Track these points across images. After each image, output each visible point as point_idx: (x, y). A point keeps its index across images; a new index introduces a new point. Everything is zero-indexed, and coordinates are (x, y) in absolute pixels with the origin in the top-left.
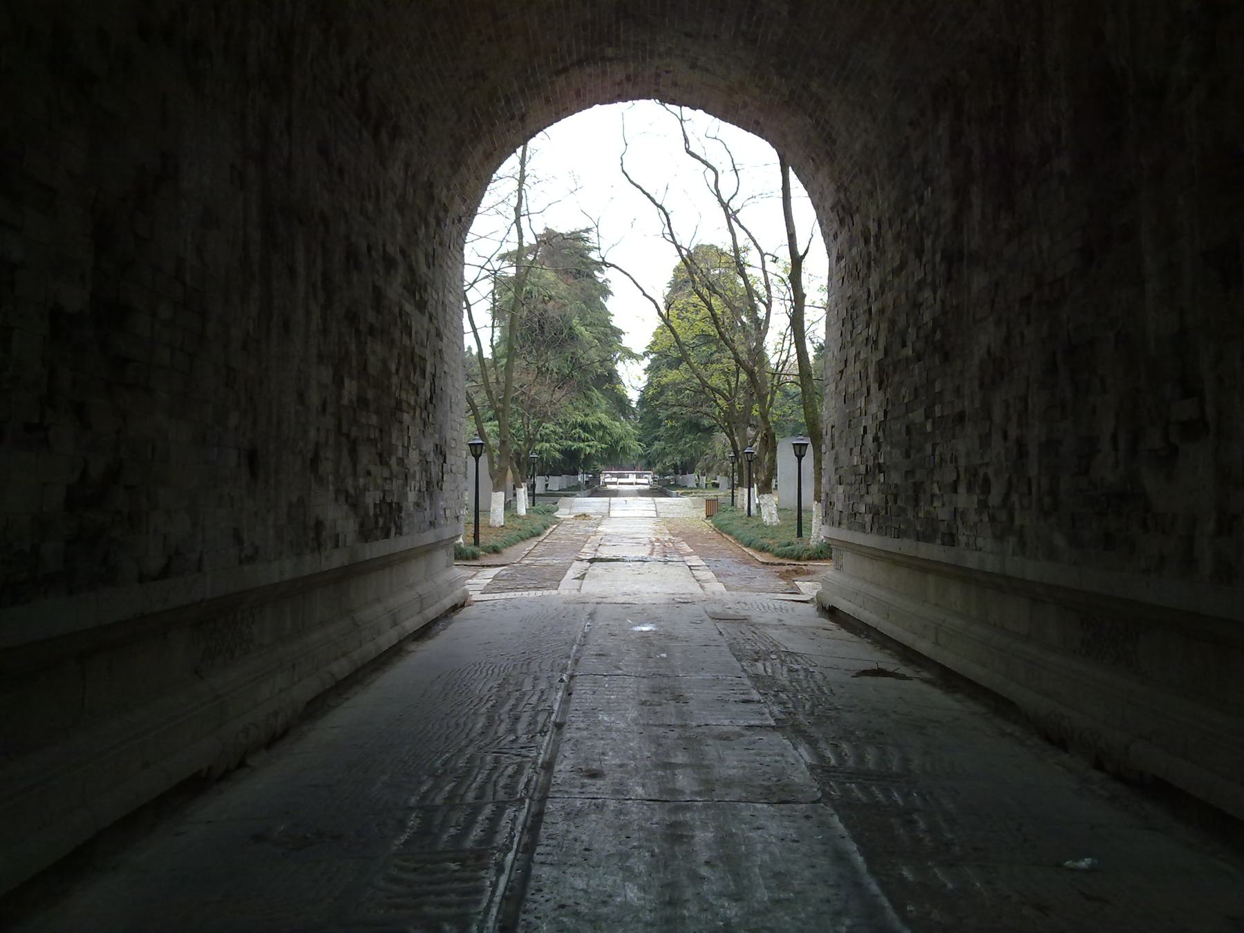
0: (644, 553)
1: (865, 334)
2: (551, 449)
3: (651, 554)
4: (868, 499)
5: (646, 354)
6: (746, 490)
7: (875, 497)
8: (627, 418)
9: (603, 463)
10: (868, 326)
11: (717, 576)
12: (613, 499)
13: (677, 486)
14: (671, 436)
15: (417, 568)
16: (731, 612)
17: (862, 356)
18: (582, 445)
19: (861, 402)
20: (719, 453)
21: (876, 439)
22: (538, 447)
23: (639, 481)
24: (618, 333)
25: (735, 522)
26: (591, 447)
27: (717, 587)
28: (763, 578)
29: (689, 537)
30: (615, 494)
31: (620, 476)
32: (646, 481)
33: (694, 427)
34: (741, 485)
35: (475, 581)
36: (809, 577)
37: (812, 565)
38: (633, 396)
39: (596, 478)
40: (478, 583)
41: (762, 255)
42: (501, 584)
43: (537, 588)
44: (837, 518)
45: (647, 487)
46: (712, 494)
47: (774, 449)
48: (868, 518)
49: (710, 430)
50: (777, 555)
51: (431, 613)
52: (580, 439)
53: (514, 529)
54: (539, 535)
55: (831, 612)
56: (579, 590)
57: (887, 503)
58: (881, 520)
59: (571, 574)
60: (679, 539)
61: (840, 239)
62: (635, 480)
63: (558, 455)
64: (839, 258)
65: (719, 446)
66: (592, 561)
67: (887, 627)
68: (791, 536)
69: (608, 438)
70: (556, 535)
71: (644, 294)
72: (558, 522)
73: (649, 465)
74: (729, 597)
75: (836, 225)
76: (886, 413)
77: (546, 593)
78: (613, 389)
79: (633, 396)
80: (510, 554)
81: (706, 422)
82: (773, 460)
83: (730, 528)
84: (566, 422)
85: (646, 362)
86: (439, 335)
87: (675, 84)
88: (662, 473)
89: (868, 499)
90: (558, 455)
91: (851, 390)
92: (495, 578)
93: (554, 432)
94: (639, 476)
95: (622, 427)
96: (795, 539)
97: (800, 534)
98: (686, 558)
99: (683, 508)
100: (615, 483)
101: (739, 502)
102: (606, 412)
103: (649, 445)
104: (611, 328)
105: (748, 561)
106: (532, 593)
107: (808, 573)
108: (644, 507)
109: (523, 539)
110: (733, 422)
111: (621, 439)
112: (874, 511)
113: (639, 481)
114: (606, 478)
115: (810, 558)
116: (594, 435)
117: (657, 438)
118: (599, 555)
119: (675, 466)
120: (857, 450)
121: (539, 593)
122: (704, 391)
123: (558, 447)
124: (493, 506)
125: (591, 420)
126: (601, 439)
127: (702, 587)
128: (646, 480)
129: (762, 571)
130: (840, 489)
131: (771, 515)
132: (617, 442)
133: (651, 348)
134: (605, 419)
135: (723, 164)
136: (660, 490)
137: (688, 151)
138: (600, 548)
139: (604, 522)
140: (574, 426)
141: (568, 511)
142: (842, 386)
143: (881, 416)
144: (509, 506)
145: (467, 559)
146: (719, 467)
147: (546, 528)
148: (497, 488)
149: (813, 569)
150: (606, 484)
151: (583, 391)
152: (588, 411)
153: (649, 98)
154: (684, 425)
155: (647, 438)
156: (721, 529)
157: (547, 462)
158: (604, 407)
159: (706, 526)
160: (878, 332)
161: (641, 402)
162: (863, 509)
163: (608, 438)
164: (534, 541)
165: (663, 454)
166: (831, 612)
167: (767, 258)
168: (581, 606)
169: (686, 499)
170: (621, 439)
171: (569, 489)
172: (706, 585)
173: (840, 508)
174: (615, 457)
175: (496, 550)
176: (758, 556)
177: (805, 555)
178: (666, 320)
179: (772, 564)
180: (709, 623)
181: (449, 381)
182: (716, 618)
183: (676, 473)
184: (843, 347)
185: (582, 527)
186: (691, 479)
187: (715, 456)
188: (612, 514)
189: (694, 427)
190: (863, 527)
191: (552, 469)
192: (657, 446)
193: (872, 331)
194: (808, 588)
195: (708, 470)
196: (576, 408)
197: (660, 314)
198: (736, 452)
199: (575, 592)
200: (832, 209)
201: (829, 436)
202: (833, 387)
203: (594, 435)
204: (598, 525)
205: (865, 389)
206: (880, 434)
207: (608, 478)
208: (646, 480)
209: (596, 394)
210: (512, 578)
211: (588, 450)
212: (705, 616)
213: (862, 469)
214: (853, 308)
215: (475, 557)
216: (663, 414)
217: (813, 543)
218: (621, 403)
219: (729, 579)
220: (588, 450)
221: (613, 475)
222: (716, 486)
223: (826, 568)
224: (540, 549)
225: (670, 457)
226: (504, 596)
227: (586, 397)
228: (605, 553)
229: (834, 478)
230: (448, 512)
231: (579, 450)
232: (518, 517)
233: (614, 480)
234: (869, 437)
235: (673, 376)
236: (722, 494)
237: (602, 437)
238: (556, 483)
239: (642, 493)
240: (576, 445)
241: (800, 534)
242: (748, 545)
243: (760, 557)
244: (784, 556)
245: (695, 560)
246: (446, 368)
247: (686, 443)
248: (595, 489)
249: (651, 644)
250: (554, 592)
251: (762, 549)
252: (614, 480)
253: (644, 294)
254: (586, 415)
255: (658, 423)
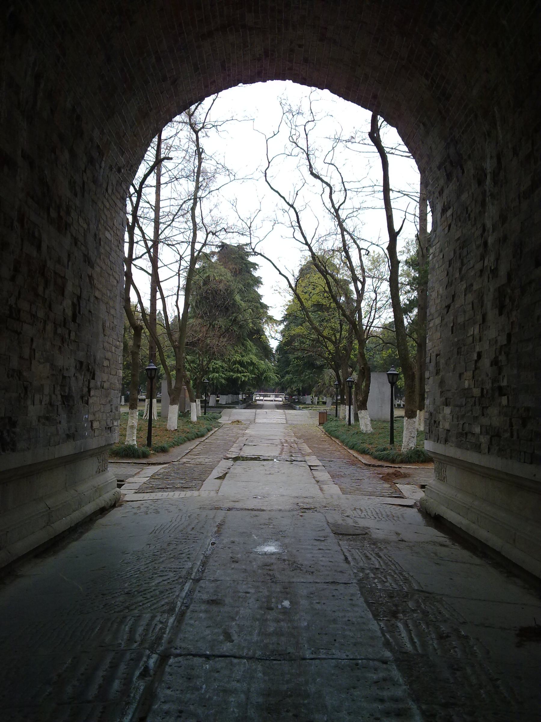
0: (275, 452)
1: (479, 266)
2: (220, 377)
3: (281, 454)
4: (485, 421)
5: (282, 322)
6: (347, 407)
7: (494, 418)
8: (269, 359)
9: (254, 388)
10: (482, 258)
11: (333, 477)
12: (258, 411)
13: (299, 403)
14: (297, 371)
15: (90, 466)
16: (350, 522)
17: (475, 287)
18: (239, 375)
19: (475, 330)
20: (327, 382)
21: (495, 362)
22: (211, 376)
23: (277, 399)
24: (266, 307)
25: (340, 429)
26: (245, 376)
27: (333, 489)
28: (370, 481)
29: (308, 439)
30: (261, 407)
31: (265, 396)
32: (281, 399)
33: (310, 365)
34: (343, 402)
35: (135, 479)
36: (406, 480)
37: (405, 468)
38: (274, 344)
39: (250, 395)
40: (135, 483)
41: (360, 250)
42: (155, 483)
43: (183, 488)
44: (443, 436)
45: (281, 403)
46: (322, 408)
47: (369, 380)
48: (484, 440)
49: (321, 368)
50: (375, 458)
51: (61, 525)
52: (238, 371)
53: (184, 431)
54: (202, 436)
55: (435, 520)
56: (217, 491)
57: (511, 425)
58: (496, 441)
59: (216, 473)
60: (301, 441)
61: (446, 192)
62: (273, 399)
63: (223, 381)
64: (444, 211)
65: (327, 378)
66: (236, 459)
67: (515, 554)
68: (385, 442)
69: (256, 371)
70: (216, 436)
71: (280, 273)
72: (219, 426)
73: (283, 390)
74: (346, 502)
75: (442, 182)
76: (509, 336)
77: (189, 493)
78: (260, 338)
79: (274, 344)
80: (176, 453)
81: (325, 354)
82: (368, 386)
83: (337, 434)
84: (229, 360)
85: (282, 327)
86: (88, 261)
87: (306, 60)
88: (291, 395)
89: (485, 421)
90: (223, 381)
91: (460, 320)
92: (152, 477)
93: (223, 368)
94: (276, 396)
95: (269, 366)
96: (388, 446)
97: (392, 442)
98: (307, 458)
99: (304, 417)
100: (262, 400)
101: (341, 415)
102: (256, 355)
103: (283, 377)
104: (261, 304)
105: (354, 463)
106: (177, 495)
107: (405, 476)
108: (278, 417)
109: (189, 440)
110: (339, 361)
111: (265, 372)
112: (495, 435)
113: (277, 399)
114: (257, 397)
115: (402, 462)
116: (247, 369)
117: (288, 373)
118: (242, 454)
119: (298, 390)
120: (469, 374)
121: (183, 494)
122: (320, 340)
123: (224, 376)
124: (170, 415)
125: (246, 359)
126: (252, 372)
127: (321, 489)
128: (281, 399)
129: (367, 473)
130: (447, 411)
131: (366, 425)
132: (262, 374)
133: (285, 318)
134: (255, 359)
135: (336, 182)
136: (289, 405)
137: (312, 174)
138: (245, 448)
139: (251, 426)
140: (235, 363)
141: (227, 418)
142: (450, 318)
143: (502, 340)
144: (184, 414)
145: (139, 457)
146: (327, 391)
147: (209, 430)
148: (173, 402)
149: (407, 471)
150: (256, 400)
151: (240, 340)
152: (244, 354)
153: (284, 79)
154: (305, 364)
155: (282, 370)
156: (330, 433)
157: (217, 387)
158: (254, 351)
159: (319, 431)
160: (497, 260)
161: (279, 348)
162: (477, 430)
163: (256, 371)
164: (197, 441)
165: (291, 382)
166: (435, 520)
167: (363, 252)
168: (212, 513)
169: (305, 412)
170: (265, 372)
171: (233, 403)
172: (325, 487)
173: (447, 426)
174: (260, 383)
175: (163, 450)
176: (360, 457)
177: (399, 459)
178: (297, 296)
179: (374, 466)
180: (332, 539)
181: (103, 307)
182: (340, 533)
183: (299, 394)
184: (449, 284)
185: (235, 430)
186: (308, 399)
187: (324, 384)
188: (257, 421)
189: (310, 365)
190: (477, 448)
191: (219, 390)
192: (288, 377)
193: (489, 261)
194: (412, 493)
195: (319, 393)
196: (236, 352)
197: (290, 286)
198: (339, 381)
199: (213, 494)
200: (439, 168)
201: (433, 363)
202: (438, 321)
203: (247, 369)
204: (247, 428)
205: (479, 317)
206: (502, 358)
207: (257, 397)
208: (281, 399)
209: (249, 343)
210: (166, 476)
211: (243, 378)
212: (328, 530)
213: (476, 392)
214: (462, 248)
215: (145, 456)
216: (291, 357)
217: (404, 450)
218: (265, 350)
219: (342, 480)
220: (243, 378)
221: (261, 395)
222: (324, 403)
223: (426, 474)
224: (200, 447)
225: (295, 384)
226: (153, 496)
227: (243, 345)
228: (248, 452)
229: (439, 400)
230: (96, 425)
231: (238, 378)
232: (191, 422)
233: (262, 398)
234: (486, 362)
235: (297, 330)
236: (329, 408)
237: (253, 370)
238: (223, 399)
239: (278, 407)
240: (235, 375)
241: (392, 442)
242: (352, 448)
243: (365, 459)
244: (380, 459)
245: (313, 461)
246: (97, 294)
247: (306, 375)
248: (249, 404)
249: (274, 581)
250: (196, 493)
251: (363, 452)
252: (262, 398)
253: (280, 273)
254: (242, 356)
255: (287, 363)
